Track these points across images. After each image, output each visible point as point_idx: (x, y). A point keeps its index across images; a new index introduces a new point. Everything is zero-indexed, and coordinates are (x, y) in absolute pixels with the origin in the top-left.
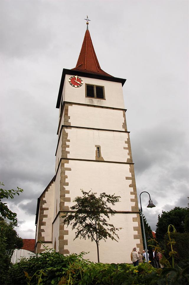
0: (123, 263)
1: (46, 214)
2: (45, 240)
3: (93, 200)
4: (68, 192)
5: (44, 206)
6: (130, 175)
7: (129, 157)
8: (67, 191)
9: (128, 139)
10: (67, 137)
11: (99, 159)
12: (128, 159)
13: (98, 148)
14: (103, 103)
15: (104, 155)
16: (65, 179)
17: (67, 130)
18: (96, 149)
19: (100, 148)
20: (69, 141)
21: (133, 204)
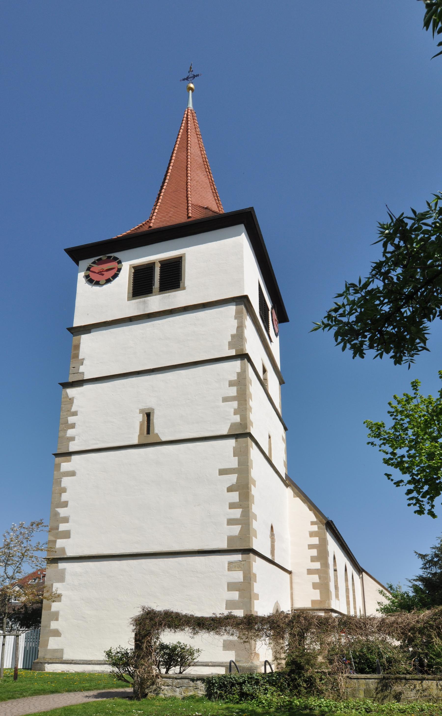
0: (133, 635)
1: (231, 350)
2: (86, 377)
3: (417, 456)
4: (66, 520)
5: (316, 578)
6: (234, 463)
7: (237, 419)
8: (237, 330)
9: (238, 374)
10: (72, 406)
11: (149, 439)
12: (233, 426)
13: (148, 415)
14: (176, 299)
15: (162, 430)
16: (61, 494)
17: (71, 392)
18: (140, 418)
19: (154, 413)
20: (75, 414)
21: (236, 530)
